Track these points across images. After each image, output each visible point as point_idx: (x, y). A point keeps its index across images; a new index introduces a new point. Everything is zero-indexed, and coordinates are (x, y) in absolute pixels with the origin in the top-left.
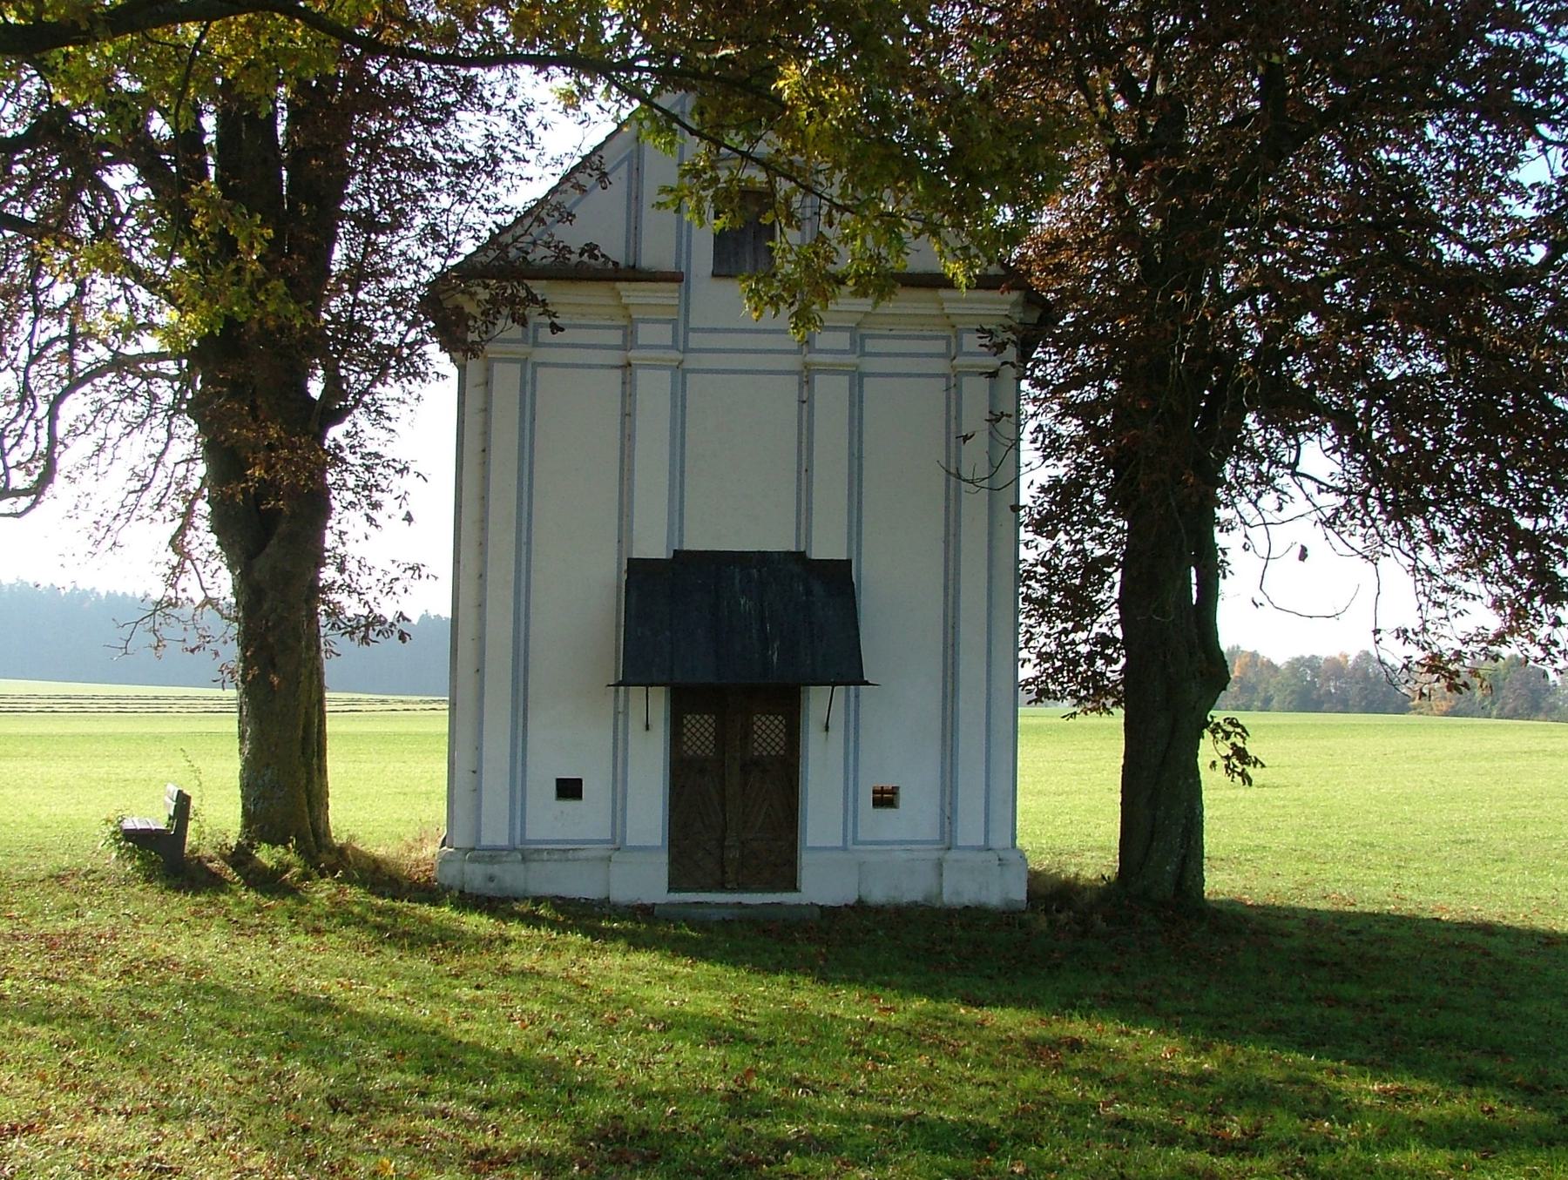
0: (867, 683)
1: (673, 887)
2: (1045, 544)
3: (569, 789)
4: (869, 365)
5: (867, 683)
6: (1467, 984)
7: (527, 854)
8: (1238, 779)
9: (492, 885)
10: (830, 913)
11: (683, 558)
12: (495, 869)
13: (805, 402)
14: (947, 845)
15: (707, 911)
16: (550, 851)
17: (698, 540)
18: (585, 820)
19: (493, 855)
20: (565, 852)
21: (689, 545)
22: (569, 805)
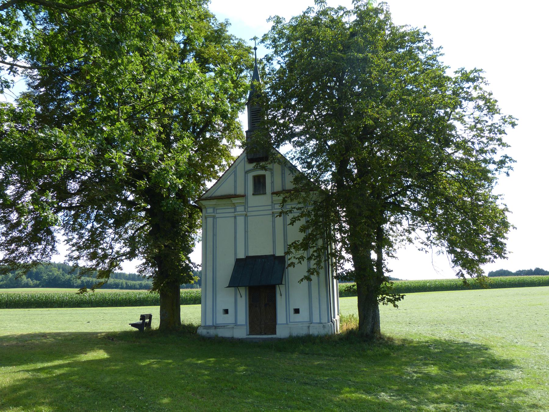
3: (226, 312)
11: (248, 258)
12: (209, 331)
13: (274, 222)
18: (229, 319)
19: (209, 327)
20: (224, 326)
22: (226, 315)
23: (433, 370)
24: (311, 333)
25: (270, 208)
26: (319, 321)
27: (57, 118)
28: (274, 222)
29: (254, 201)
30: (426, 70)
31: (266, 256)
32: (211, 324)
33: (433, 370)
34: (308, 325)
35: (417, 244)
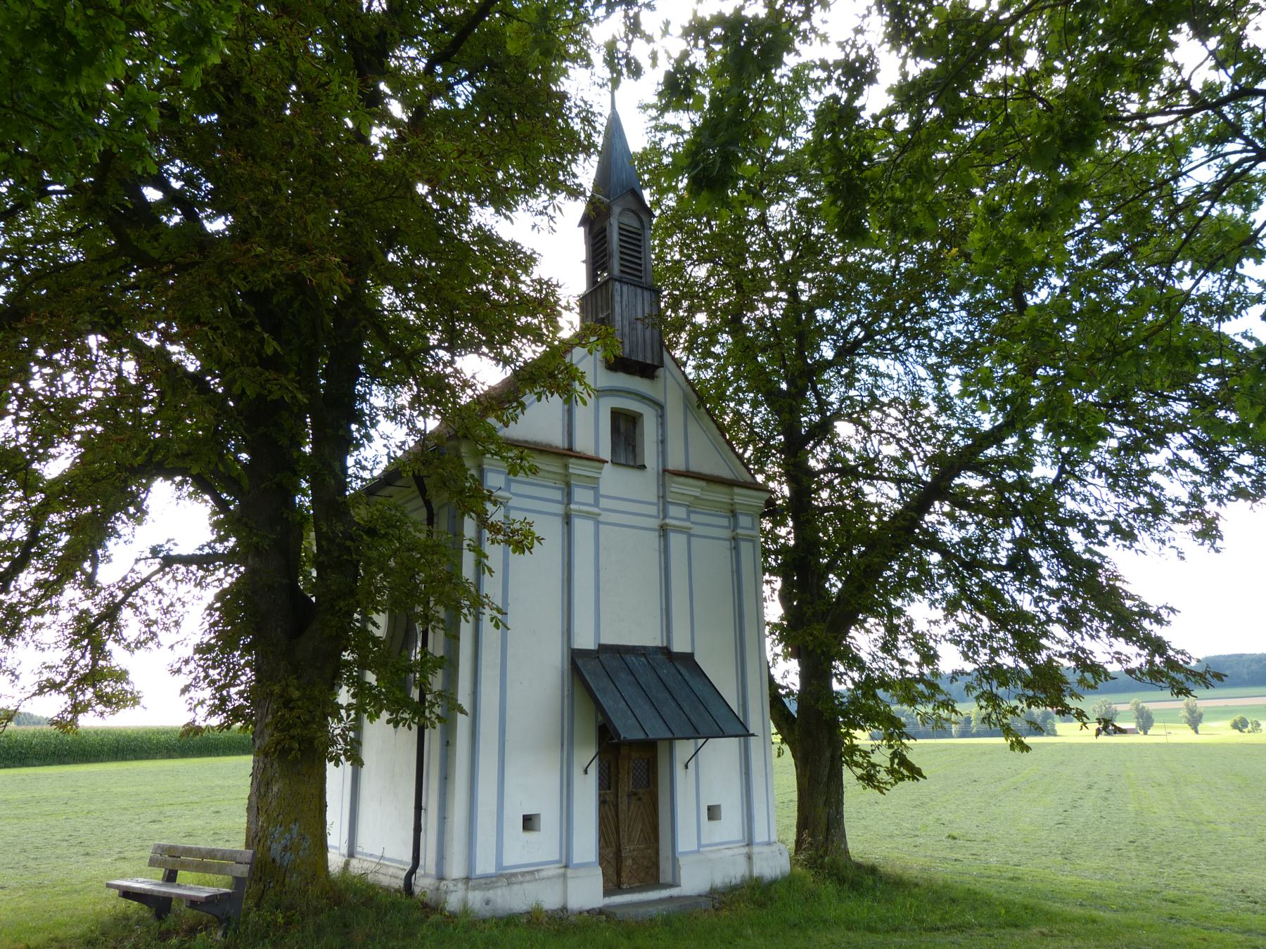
0: (753, 735)
1: (607, 893)
2: (399, 401)
3: (529, 822)
4: (697, 530)
5: (753, 735)
6: (1169, 474)
7: (505, 877)
8: (176, 666)
9: (488, 907)
10: (723, 899)
11: (603, 648)
12: (490, 894)
13: (665, 551)
14: (564, 864)
15: (641, 910)
16: (523, 874)
17: (609, 639)
18: (539, 848)
19: (489, 881)
20: (531, 873)
21: (603, 641)
22: (530, 836)
23: (1007, 15)
24: (756, 873)
25: (653, 510)
26: (766, 839)
27: (409, 290)
28: (665, 551)
29: (614, 480)
30: (911, 445)
31: (644, 648)
32: (491, 869)
33: (1007, 15)
34: (745, 850)
35: (538, 272)
